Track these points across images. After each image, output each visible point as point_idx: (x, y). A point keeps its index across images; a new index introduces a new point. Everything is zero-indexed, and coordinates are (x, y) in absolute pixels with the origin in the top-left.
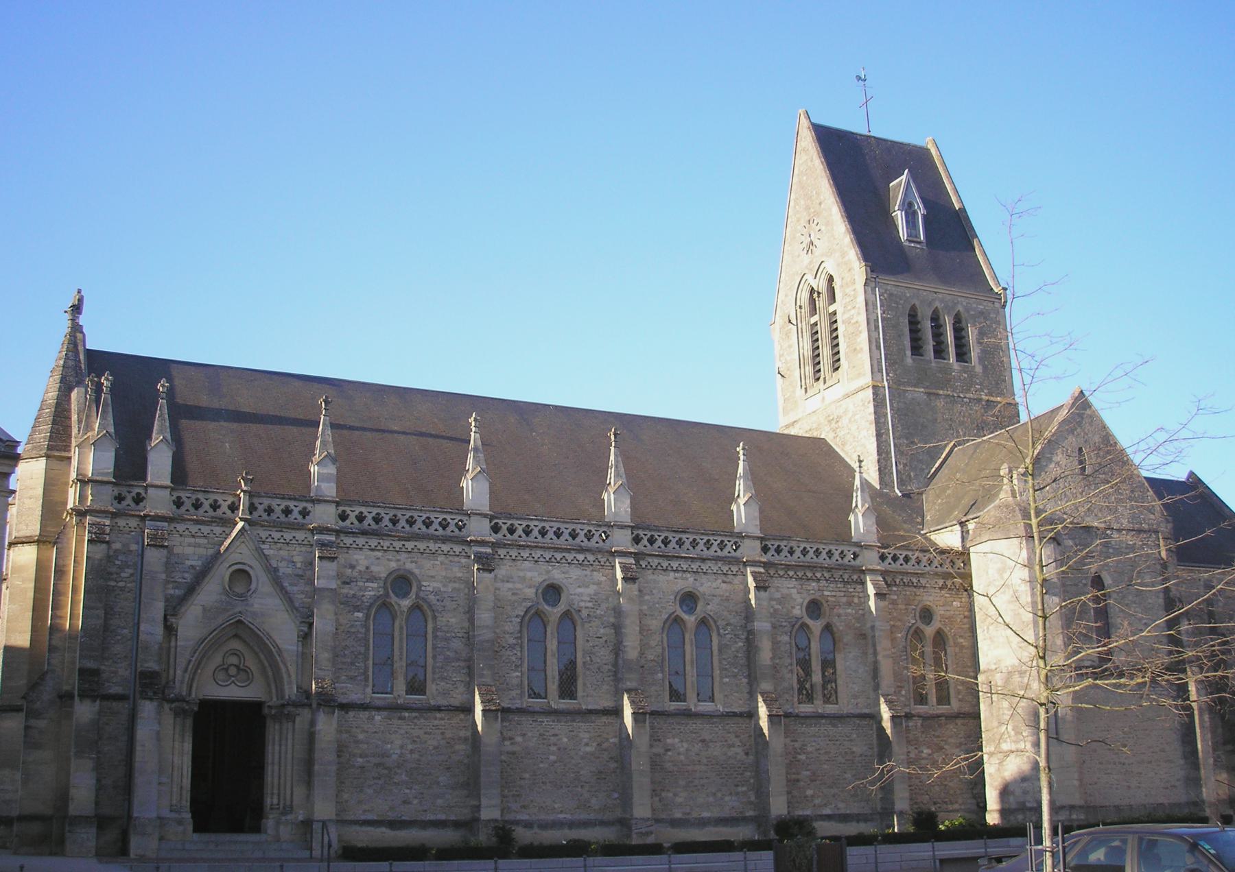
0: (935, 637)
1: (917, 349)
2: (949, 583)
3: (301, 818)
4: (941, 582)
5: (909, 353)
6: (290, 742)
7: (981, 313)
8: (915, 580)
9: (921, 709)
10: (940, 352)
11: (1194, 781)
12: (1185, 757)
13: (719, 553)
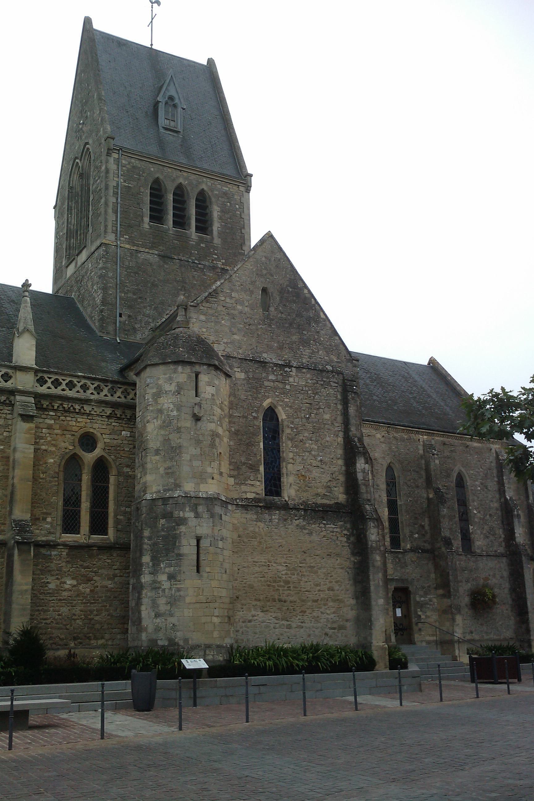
0: (387, 469)
1: (157, 215)
2: (309, 426)
4: (109, 411)
5: (147, 219)
7: (225, 194)
8: (77, 407)
9: (69, 538)
10: (180, 221)
11: (364, 622)
12: (357, 598)
13: (109, 398)
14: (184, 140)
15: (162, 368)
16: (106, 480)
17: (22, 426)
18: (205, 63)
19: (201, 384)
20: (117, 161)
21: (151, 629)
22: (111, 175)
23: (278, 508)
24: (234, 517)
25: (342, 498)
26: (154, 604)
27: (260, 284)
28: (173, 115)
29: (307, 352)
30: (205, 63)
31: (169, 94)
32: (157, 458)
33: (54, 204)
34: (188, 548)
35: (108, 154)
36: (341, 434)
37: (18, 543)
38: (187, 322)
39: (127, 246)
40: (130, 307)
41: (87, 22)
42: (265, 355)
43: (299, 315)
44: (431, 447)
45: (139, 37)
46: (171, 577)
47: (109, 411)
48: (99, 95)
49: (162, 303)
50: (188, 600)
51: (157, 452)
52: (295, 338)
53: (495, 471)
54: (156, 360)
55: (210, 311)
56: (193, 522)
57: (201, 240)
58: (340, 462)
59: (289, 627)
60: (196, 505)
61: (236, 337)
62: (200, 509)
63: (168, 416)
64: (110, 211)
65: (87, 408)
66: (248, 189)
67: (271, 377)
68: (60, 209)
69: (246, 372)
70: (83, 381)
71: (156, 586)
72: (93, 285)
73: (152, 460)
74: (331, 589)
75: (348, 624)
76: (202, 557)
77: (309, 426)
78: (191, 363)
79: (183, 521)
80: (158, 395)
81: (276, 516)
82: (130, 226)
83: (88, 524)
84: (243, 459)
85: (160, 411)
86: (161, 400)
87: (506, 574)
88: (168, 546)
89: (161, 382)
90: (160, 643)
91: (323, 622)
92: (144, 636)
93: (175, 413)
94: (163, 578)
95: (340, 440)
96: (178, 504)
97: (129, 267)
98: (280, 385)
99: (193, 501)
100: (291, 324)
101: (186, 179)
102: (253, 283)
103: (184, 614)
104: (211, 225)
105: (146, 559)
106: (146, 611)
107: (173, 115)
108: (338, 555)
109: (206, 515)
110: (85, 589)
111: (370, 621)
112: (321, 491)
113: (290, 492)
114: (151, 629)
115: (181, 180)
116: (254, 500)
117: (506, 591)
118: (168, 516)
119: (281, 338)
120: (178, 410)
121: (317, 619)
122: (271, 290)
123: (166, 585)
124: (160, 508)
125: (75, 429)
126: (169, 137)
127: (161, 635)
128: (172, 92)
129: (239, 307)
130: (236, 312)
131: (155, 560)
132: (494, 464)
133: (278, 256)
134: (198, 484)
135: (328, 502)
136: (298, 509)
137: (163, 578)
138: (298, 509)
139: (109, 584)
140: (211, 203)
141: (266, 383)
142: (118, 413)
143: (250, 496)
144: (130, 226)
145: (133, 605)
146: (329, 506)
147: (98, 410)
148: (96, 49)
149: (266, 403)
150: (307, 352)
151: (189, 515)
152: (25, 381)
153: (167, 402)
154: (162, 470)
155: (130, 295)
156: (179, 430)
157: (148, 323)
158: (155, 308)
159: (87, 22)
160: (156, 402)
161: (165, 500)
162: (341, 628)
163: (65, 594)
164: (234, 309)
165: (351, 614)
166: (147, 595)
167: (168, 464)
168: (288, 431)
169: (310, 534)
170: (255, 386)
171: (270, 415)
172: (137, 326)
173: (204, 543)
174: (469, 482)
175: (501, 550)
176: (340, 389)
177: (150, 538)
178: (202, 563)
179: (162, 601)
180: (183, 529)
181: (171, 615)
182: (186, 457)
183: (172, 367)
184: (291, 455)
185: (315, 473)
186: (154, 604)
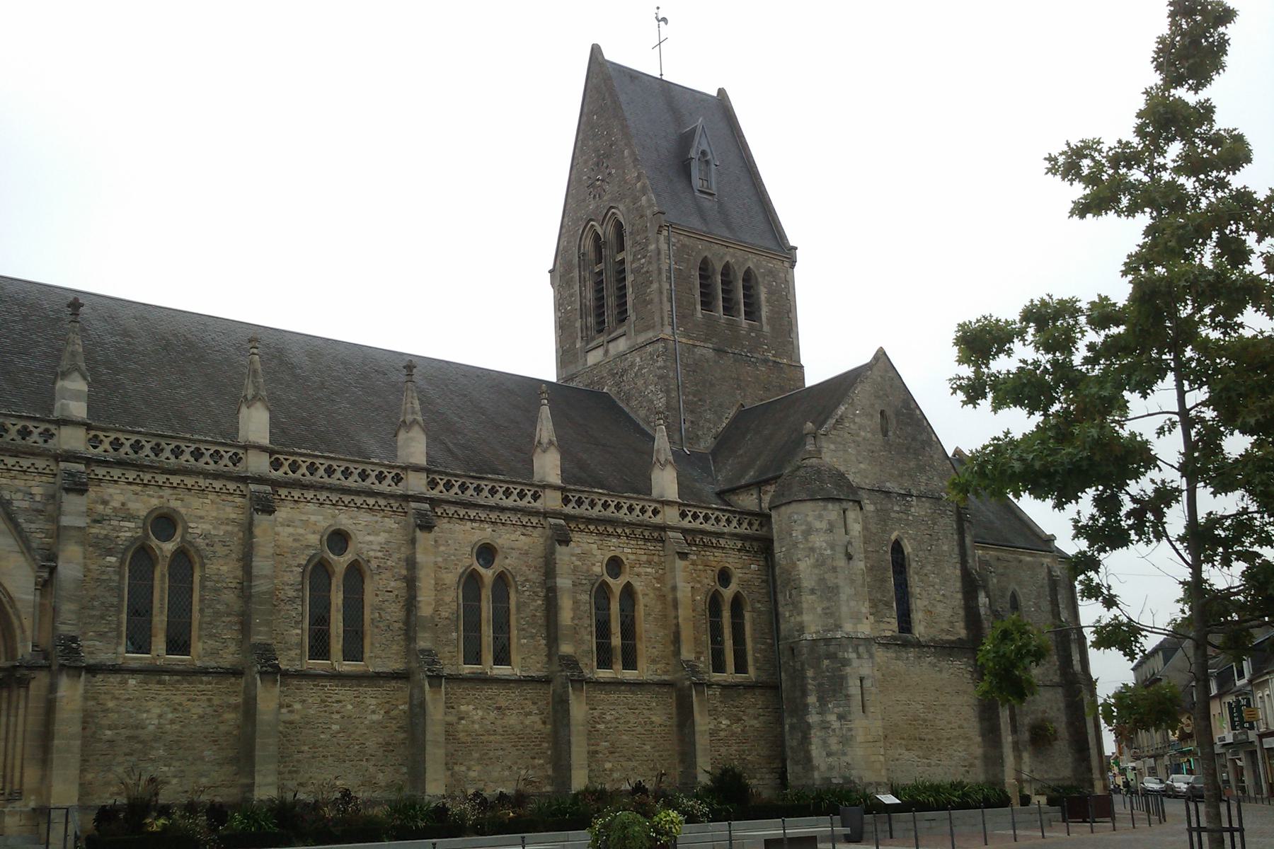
1: (707, 304)
3: (32, 804)
4: (739, 544)
5: (699, 307)
6: (21, 719)
9: (717, 677)
13: (738, 530)
14: (720, 204)
15: (809, 504)
16: (742, 617)
17: (680, 564)
18: (715, 94)
19: (850, 521)
20: (668, 239)
21: (823, 767)
22: (663, 256)
23: (913, 646)
24: (881, 655)
25: (963, 633)
26: (825, 742)
27: (878, 408)
28: (706, 174)
29: (924, 479)
30: (715, 94)
31: (701, 148)
32: (813, 597)
33: (551, 267)
34: (854, 688)
35: (659, 232)
36: (958, 566)
37: (695, 684)
38: (818, 453)
39: (684, 340)
40: (692, 412)
41: (596, 51)
42: (888, 484)
43: (914, 439)
44: (987, 563)
45: (646, 64)
46: (841, 717)
47: (739, 544)
48: (633, 153)
49: (720, 405)
50: (859, 739)
51: (813, 591)
52: (912, 464)
53: (1047, 589)
54: (804, 496)
55: (839, 439)
56: (855, 663)
57: (752, 328)
58: (960, 596)
59: (929, 765)
60: (857, 646)
61: (862, 466)
62: (861, 649)
63: (822, 554)
64: (665, 299)
65: (722, 542)
66: (793, 263)
67: (897, 508)
68: (561, 275)
69: (875, 504)
70: (717, 513)
71: (825, 726)
72: (646, 384)
73: (807, 600)
74: (960, 727)
75: (977, 762)
76: (866, 698)
77: (931, 559)
78: (839, 500)
79: (846, 662)
80: (808, 532)
81: (912, 653)
82: (684, 317)
83: (639, 652)
84: (879, 596)
85: (812, 549)
86: (812, 538)
87: (1062, 705)
88: (835, 687)
89: (810, 519)
90: (835, 781)
91: (955, 761)
92: (816, 775)
93: (829, 552)
94: (832, 718)
95: (958, 572)
96: (840, 643)
97: (687, 365)
98: (905, 517)
99: (855, 642)
100: (908, 449)
101: (733, 256)
102: (872, 405)
103: (858, 753)
104: (759, 309)
105: (812, 699)
106: (816, 751)
107: (706, 174)
108: (965, 692)
109: (866, 656)
110: (737, 728)
111: (1002, 758)
112: (945, 626)
113: (920, 629)
114: (823, 767)
115: (728, 258)
116: (892, 637)
117: (1063, 725)
118: (832, 656)
119: (900, 465)
120: (832, 548)
121: (951, 757)
122: (889, 412)
123: (836, 725)
124: (822, 648)
125: (714, 564)
126: (707, 203)
127: (835, 773)
128: (705, 147)
129: (863, 434)
130: (859, 439)
131: (822, 701)
132: (1046, 581)
133: (891, 374)
134: (855, 624)
135: (949, 637)
136: (929, 647)
137: (832, 718)
138: (929, 647)
139: (755, 723)
140: (757, 282)
141: (893, 515)
142: (747, 545)
143: (888, 634)
144: (684, 317)
145: (795, 743)
146: (953, 642)
147: (731, 543)
148: (609, 89)
149: (893, 537)
150: (924, 479)
151: (853, 656)
152: (671, 516)
153: (818, 541)
154: (819, 610)
155: (691, 397)
156: (834, 569)
157: (709, 429)
158: (715, 412)
159: (596, 51)
160: (807, 540)
161: (827, 641)
162: (971, 765)
163: (722, 734)
164: (858, 435)
165: (979, 751)
166: (816, 736)
167: (826, 604)
168: (914, 565)
169: (941, 671)
170: (883, 517)
171: (897, 547)
172: (700, 433)
173: (867, 683)
174: (1023, 602)
175: (1057, 679)
176: (954, 518)
177: (814, 679)
178: (868, 703)
179: (833, 741)
180: (848, 669)
181: (845, 754)
182: (843, 597)
183: (821, 504)
184: (918, 590)
185: (940, 608)
186: (825, 742)
